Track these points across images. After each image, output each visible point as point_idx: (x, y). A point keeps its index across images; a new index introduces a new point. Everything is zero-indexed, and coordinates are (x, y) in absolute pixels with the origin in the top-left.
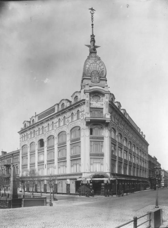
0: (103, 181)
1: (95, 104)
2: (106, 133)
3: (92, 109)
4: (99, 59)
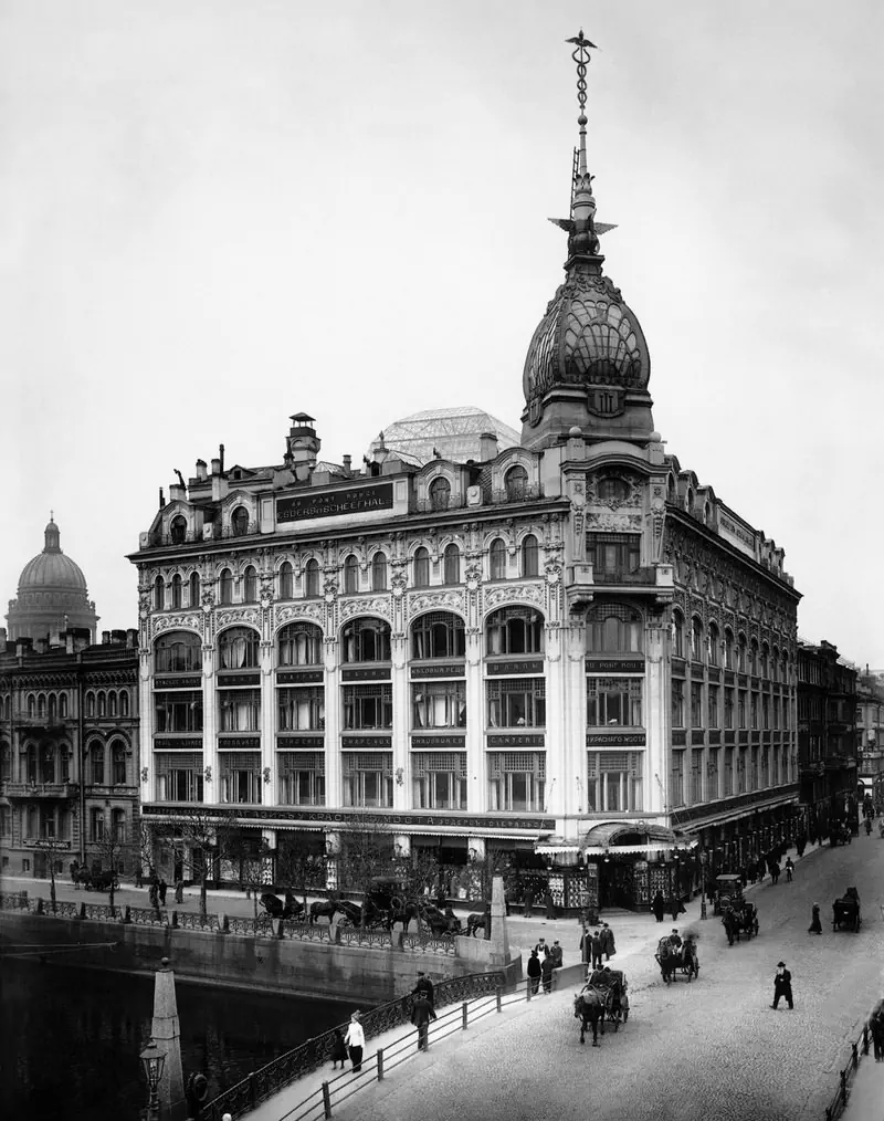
0: (639, 856)
1: (615, 518)
2: (655, 648)
3: (597, 543)
4: (616, 297)
